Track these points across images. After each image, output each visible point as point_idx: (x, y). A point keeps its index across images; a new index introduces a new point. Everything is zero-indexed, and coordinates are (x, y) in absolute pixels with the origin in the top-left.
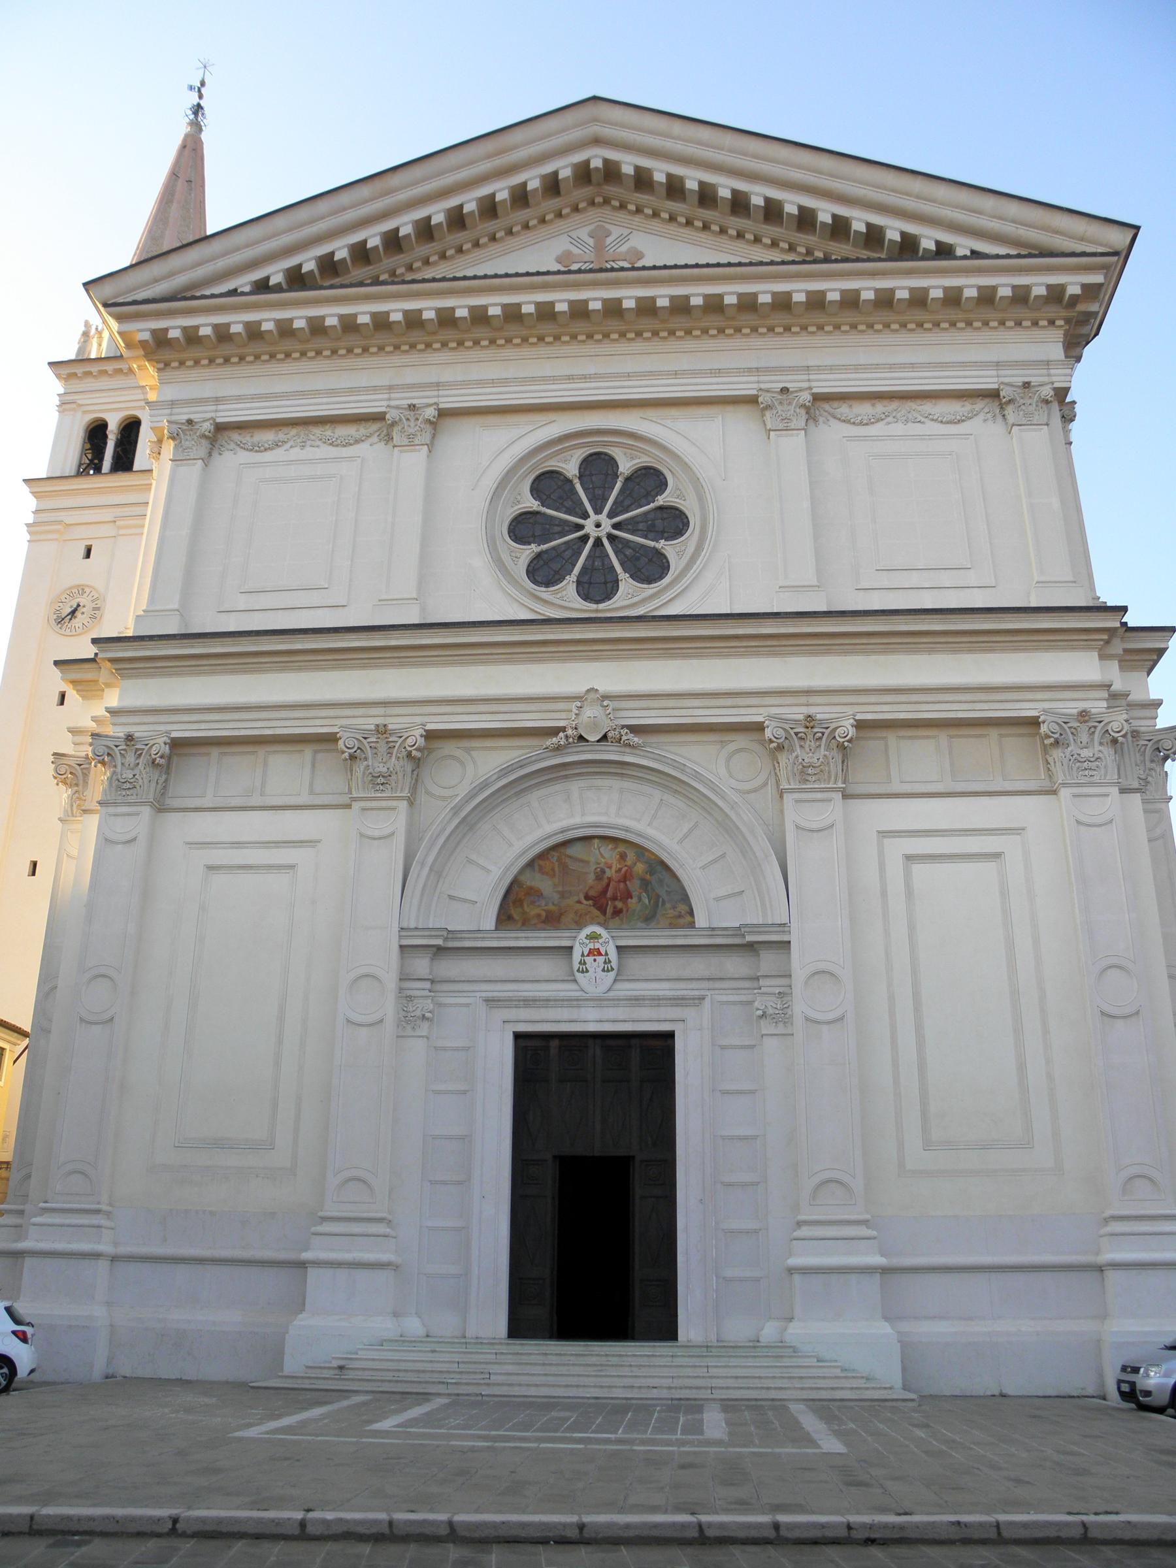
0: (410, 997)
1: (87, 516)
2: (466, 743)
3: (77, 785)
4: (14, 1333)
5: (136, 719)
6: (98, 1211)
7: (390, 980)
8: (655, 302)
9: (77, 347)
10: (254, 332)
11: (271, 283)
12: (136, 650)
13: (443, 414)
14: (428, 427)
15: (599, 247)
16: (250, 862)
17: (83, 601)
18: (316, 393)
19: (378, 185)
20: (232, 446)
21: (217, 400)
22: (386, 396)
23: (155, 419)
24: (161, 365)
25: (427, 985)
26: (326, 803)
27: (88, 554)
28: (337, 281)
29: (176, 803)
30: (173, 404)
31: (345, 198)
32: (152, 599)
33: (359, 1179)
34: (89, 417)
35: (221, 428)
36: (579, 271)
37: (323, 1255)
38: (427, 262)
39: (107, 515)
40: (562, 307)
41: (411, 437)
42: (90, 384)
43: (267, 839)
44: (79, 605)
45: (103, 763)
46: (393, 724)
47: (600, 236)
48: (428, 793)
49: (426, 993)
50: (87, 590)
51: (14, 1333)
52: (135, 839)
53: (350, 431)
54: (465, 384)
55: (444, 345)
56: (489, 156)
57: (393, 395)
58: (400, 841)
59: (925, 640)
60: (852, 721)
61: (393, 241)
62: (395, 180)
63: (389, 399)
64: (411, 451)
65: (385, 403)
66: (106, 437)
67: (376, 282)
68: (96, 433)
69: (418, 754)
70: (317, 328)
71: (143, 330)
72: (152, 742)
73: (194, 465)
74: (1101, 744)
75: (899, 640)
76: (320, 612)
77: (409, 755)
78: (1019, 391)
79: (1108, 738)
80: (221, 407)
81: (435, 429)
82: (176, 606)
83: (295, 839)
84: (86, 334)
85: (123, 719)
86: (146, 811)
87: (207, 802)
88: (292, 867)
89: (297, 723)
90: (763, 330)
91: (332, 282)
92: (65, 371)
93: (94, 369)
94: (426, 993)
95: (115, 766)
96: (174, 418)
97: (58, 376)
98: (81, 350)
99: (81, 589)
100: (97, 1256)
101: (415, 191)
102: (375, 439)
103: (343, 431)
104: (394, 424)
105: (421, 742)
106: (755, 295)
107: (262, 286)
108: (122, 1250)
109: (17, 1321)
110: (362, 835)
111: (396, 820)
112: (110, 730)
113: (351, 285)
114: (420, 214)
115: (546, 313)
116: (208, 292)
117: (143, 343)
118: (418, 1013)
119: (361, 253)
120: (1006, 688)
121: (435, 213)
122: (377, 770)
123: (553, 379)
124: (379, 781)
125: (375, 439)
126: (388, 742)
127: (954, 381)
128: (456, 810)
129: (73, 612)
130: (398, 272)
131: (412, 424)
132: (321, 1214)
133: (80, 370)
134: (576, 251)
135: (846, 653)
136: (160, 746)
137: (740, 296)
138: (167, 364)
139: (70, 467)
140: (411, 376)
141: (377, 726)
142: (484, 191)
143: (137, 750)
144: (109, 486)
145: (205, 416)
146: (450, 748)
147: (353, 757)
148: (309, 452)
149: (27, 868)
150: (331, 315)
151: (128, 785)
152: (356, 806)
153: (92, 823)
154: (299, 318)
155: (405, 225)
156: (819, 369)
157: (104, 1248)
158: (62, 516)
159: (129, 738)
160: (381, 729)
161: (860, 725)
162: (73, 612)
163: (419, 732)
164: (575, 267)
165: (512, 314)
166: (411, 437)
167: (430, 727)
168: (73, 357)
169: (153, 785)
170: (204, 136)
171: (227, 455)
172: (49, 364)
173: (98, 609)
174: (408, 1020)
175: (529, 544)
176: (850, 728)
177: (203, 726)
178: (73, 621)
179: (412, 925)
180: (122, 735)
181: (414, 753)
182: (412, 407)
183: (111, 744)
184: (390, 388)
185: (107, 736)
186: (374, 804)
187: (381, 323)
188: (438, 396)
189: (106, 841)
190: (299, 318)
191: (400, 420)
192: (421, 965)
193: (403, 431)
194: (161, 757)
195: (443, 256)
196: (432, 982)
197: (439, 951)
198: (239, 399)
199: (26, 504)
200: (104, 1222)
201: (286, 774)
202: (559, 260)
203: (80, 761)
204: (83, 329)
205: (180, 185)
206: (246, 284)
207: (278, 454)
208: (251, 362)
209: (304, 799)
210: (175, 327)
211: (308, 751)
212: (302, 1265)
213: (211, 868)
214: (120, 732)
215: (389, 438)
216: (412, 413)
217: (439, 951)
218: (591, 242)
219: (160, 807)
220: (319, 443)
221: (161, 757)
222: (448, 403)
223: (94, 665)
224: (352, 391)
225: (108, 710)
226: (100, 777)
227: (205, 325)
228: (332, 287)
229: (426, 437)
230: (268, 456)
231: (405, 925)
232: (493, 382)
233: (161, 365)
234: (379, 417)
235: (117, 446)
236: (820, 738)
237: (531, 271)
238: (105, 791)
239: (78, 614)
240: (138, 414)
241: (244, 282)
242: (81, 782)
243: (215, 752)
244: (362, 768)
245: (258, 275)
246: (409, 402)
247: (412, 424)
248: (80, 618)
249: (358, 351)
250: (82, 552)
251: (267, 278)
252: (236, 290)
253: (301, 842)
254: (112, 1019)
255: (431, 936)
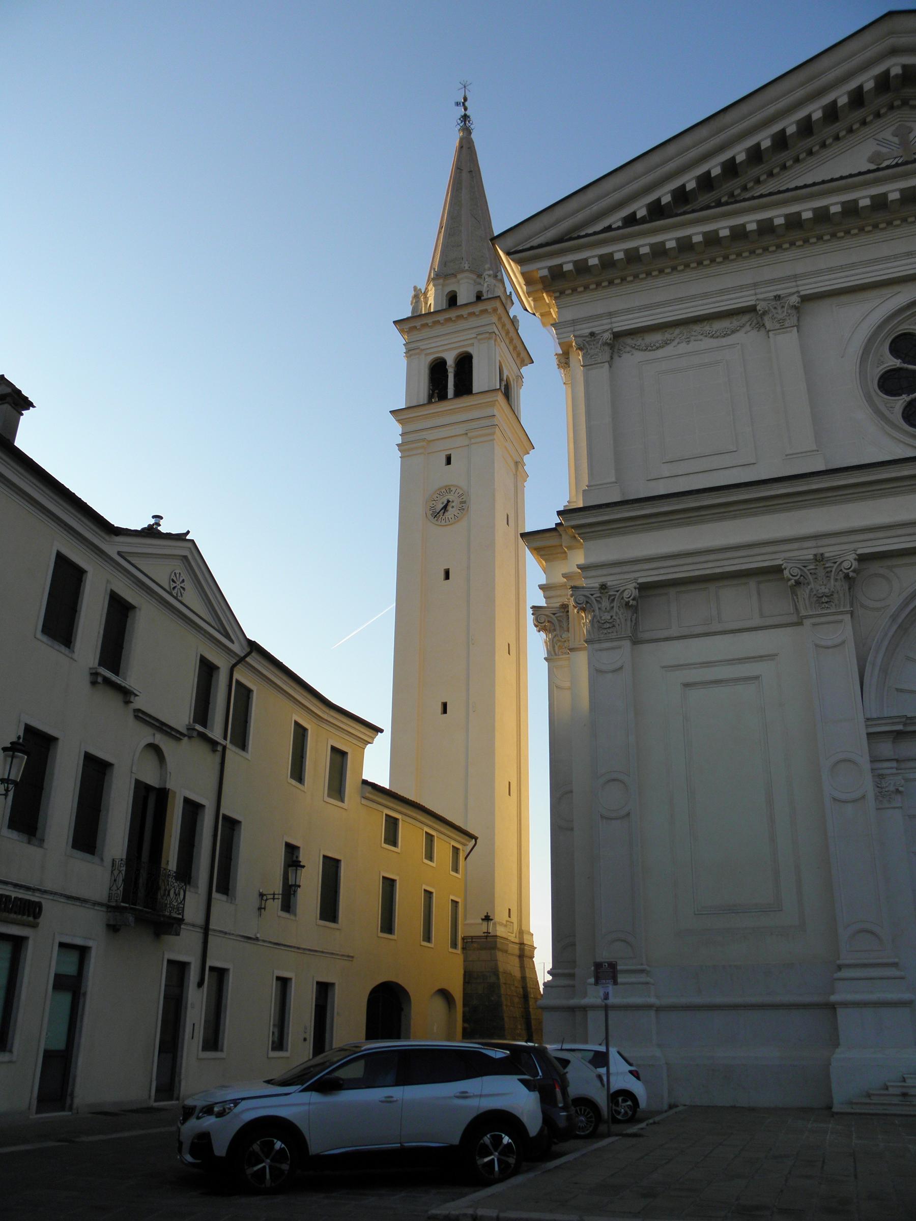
0: (882, 775)
1: (443, 433)
2: (889, 563)
3: (555, 630)
4: (631, 1072)
5: (605, 571)
6: (642, 971)
7: (864, 761)
8: (718, 234)
9: (411, 308)
10: (633, 257)
11: (638, 217)
12: (595, 516)
13: (806, 299)
14: (794, 312)
15: (905, 143)
16: (720, 677)
17: (451, 498)
18: (693, 298)
19: (714, 125)
20: (628, 349)
21: (610, 315)
22: (753, 292)
23: (561, 336)
24: (557, 294)
25: (894, 764)
26: (777, 623)
27: (449, 461)
28: (688, 208)
29: (647, 636)
30: (574, 322)
31: (688, 140)
32: (591, 474)
33: (867, 931)
34: (430, 358)
35: (617, 336)
36: (888, 167)
37: (849, 997)
38: (758, 181)
39: (460, 429)
40: (671, 244)
41: (781, 321)
42: (426, 333)
43: (731, 657)
44: (448, 501)
45: (584, 609)
46: (829, 552)
47: (903, 134)
48: (862, 606)
49: (894, 771)
50: (454, 489)
51: (631, 1072)
52: (621, 668)
53: (725, 324)
54: (818, 273)
55: (792, 244)
56: (802, 85)
57: (758, 291)
58: (850, 649)
59: (732, 509)
60: (635, 584)
61: (731, 168)
62: (728, 118)
63: (756, 294)
64: (784, 333)
65: (754, 298)
66: (446, 371)
67: (719, 204)
68: (437, 369)
69: (634, 603)
70: (685, 245)
71: (541, 269)
72: (622, 589)
73: (602, 367)
74: (836, 580)
75: (851, 491)
76: (734, 470)
77: (627, 604)
78: (588, 339)
79: (841, 575)
80: (614, 320)
81: (798, 312)
82: (613, 479)
83: (753, 655)
84: (416, 297)
85: (593, 573)
86: (627, 644)
87: (674, 632)
88: (757, 678)
89: (742, 560)
90: (813, 240)
91: (685, 209)
92: (406, 326)
93: (429, 321)
94: (894, 771)
95: (594, 611)
96: (577, 333)
97: (401, 331)
98: (414, 310)
99: (448, 489)
100: (649, 1007)
101: (745, 124)
102: (748, 328)
103: (718, 325)
104: (765, 313)
105: (636, 593)
106: (663, 243)
107: (631, 220)
108: (666, 1001)
109: (630, 1064)
110: (817, 646)
111: (844, 631)
112: (582, 582)
113: (702, 209)
114: (750, 142)
115: (822, 216)
116: (590, 231)
117: (543, 279)
118: (892, 788)
119: (706, 182)
120: (785, 541)
121: (763, 140)
122: (820, 591)
123: (896, 257)
124: (824, 600)
125: (748, 328)
126: (825, 568)
127: (728, 302)
128: (894, 618)
129: (445, 508)
130: (737, 192)
131: (780, 311)
132: (839, 962)
133: (418, 323)
134: (884, 150)
135: (735, 517)
136: (630, 591)
137: (759, 222)
138: (562, 293)
139: (423, 397)
140: (768, 273)
141: (815, 555)
142: (801, 114)
143: (610, 596)
144: (455, 409)
145: (602, 327)
146: (875, 567)
147: (798, 583)
148: (693, 346)
149: (439, 708)
150: (696, 232)
151: (608, 625)
152: (807, 622)
153: (581, 661)
154: (670, 239)
155: (739, 153)
156: (804, 276)
157: (652, 1000)
158: (424, 435)
159: (603, 587)
160: (819, 557)
161: (863, 559)
162: (445, 508)
163: (631, 586)
164: (884, 165)
165: (822, 216)
166: (781, 321)
167: (860, 552)
168: (410, 315)
169: (629, 623)
170: (473, 136)
171: (626, 356)
172: (394, 322)
173: (464, 502)
174: (882, 794)
175: (900, 395)
176: (853, 562)
177: (662, 571)
178: (446, 514)
179: (875, 716)
180: (597, 585)
181: (851, 574)
182: (778, 298)
183: (587, 594)
184: (755, 285)
185: (583, 588)
186: (823, 619)
187: (712, 240)
188: (797, 286)
189: (596, 672)
190: (670, 239)
191: (769, 310)
192: (886, 748)
193: (773, 318)
194: (633, 599)
195: (771, 175)
196: (897, 760)
197: (898, 735)
198: (629, 311)
199: (395, 430)
200: (648, 979)
201: (736, 604)
202: (871, 160)
203: (554, 611)
204: (413, 293)
205: (465, 175)
206: (617, 221)
207: (669, 350)
208: (632, 281)
209: (756, 621)
210: (567, 262)
211: (752, 583)
212: (832, 1007)
213: (687, 685)
214: (595, 583)
215: (760, 326)
216: (778, 303)
217: (898, 735)
218: (896, 140)
219: (636, 642)
220: (701, 337)
221: (633, 599)
222: (808, 288)
223: (554, 534)
224: (722, 292)
225: (579, 567)
226: (582, 623)
227: (592, 257)
228: (685, 213)
229: (794, 320)
230: (660, 353)
231: (869, 716)
232: (842, 268)
233: (557, 294)
234: (752, 309)
235: (456, 376)
236: (613, 600)
237: (844, 175)
238: (588, 631)
239: (449, 508)
240: (469, 349)
241: (615, 219)
242: (558, 628)
243: (672, 591)
244: (808, 591)
245: (625, 212)
246: (775, 293)
247: (780, 311)
248: (451, 512)
249: (593, 286)
250: (444, 461)
251: (634, 214)
252: (610, 226)
253: (761, 657)
254: (628, 814)
255: (893, 724)
